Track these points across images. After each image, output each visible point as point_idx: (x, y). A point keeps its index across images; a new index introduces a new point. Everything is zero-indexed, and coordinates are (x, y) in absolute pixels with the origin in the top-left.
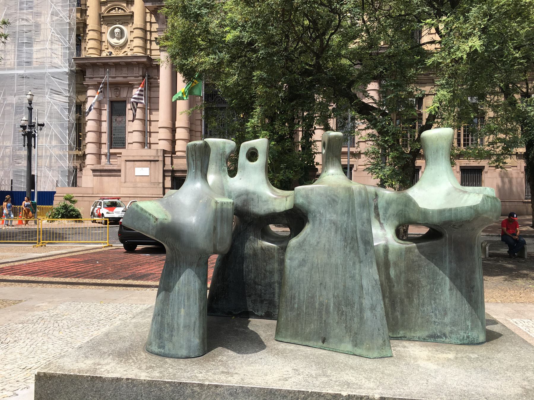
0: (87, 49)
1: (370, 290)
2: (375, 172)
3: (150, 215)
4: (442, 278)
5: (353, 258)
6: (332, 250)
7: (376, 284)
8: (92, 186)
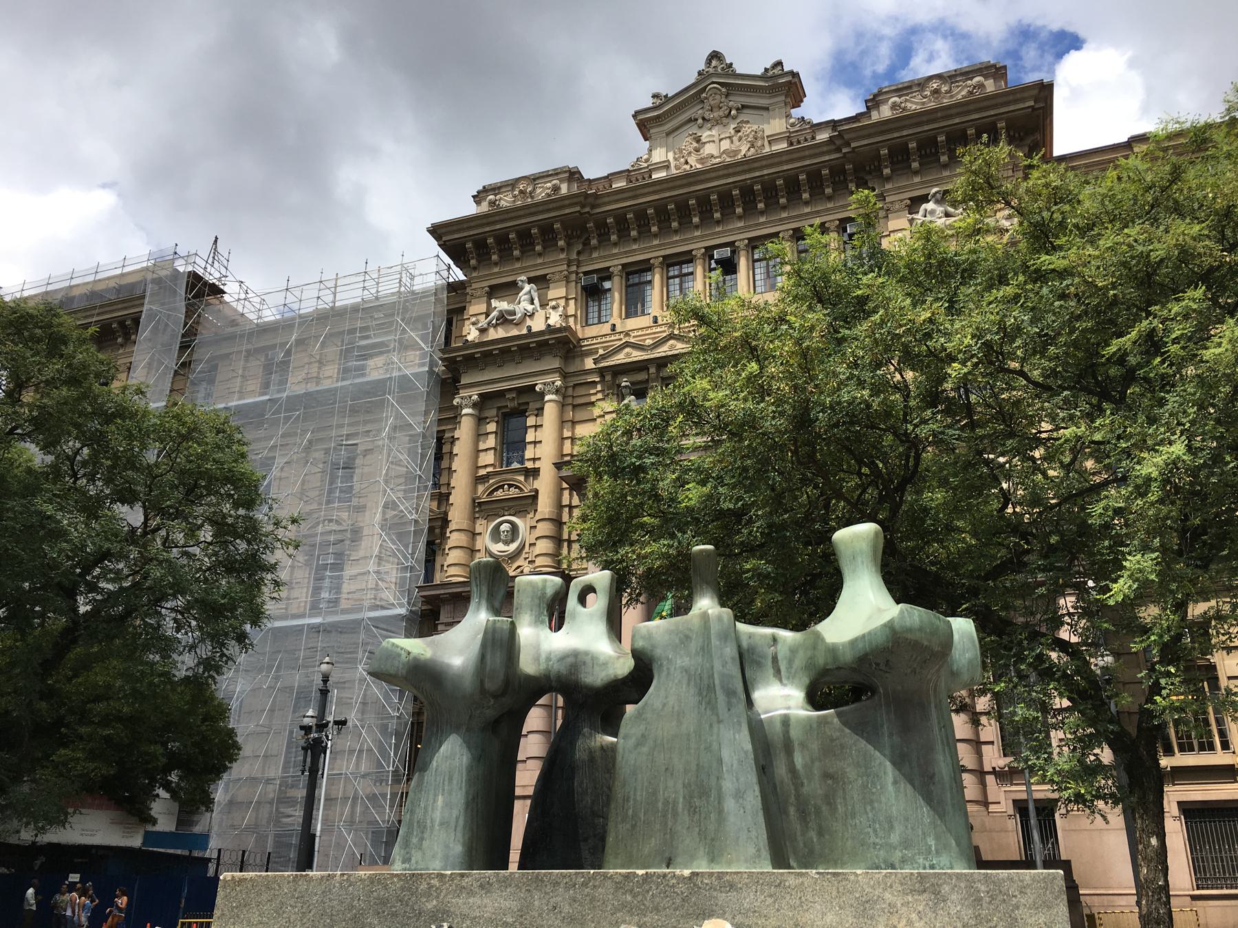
0: (445, 568)
1: (735, 766)
3: (402, 649)
4: (880, 764)
7: (747, 757)
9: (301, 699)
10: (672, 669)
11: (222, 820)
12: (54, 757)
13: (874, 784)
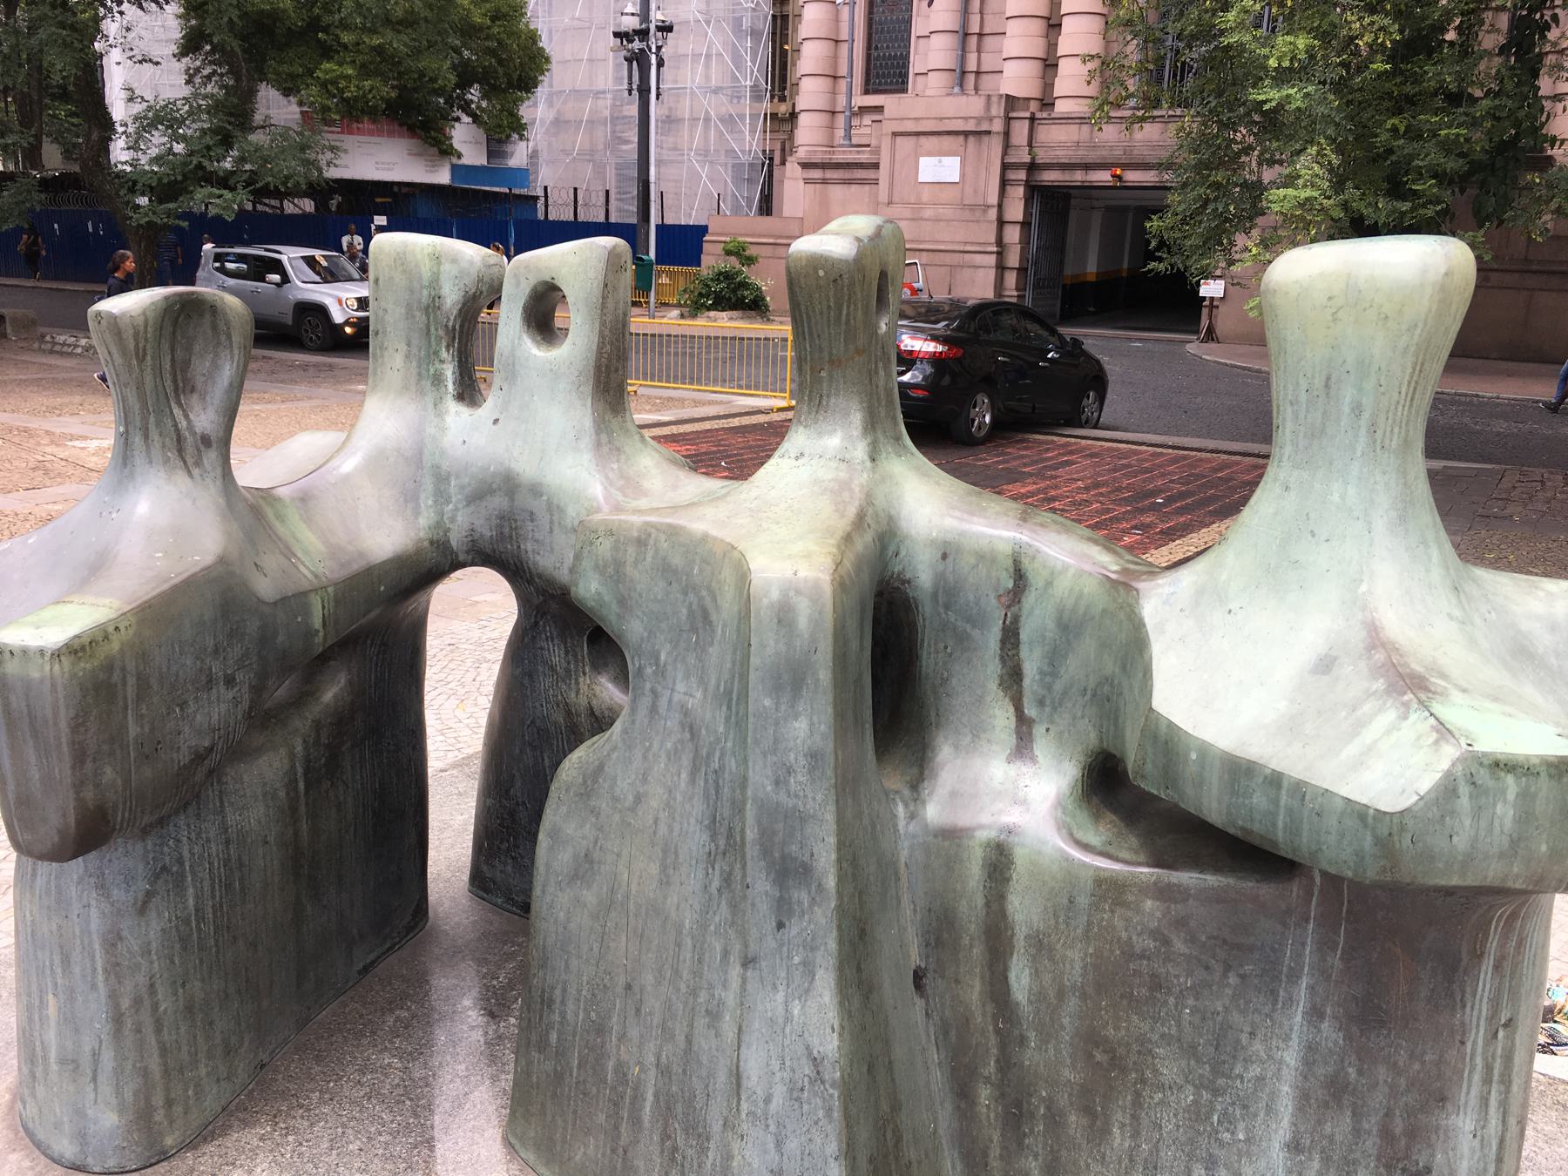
7: (818, 1077)
10: (663, 703)
11: (550, 145)
12: (318, 73)
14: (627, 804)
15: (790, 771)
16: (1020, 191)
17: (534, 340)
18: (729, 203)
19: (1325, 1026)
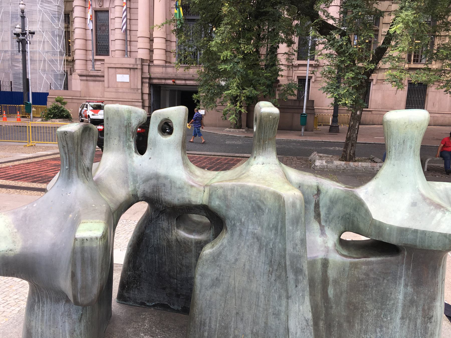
2: (330, 91)
5: (279, 291)
6: (254, 273)
8: (79, 90)
9: (13, 16)
10: (244, 232)
13: (385, 316)
14: (232, 262)
15: (296, 245)
16: (147, 85)
17: (161, 135)
18: (53, 86)
19: (409, 288)
